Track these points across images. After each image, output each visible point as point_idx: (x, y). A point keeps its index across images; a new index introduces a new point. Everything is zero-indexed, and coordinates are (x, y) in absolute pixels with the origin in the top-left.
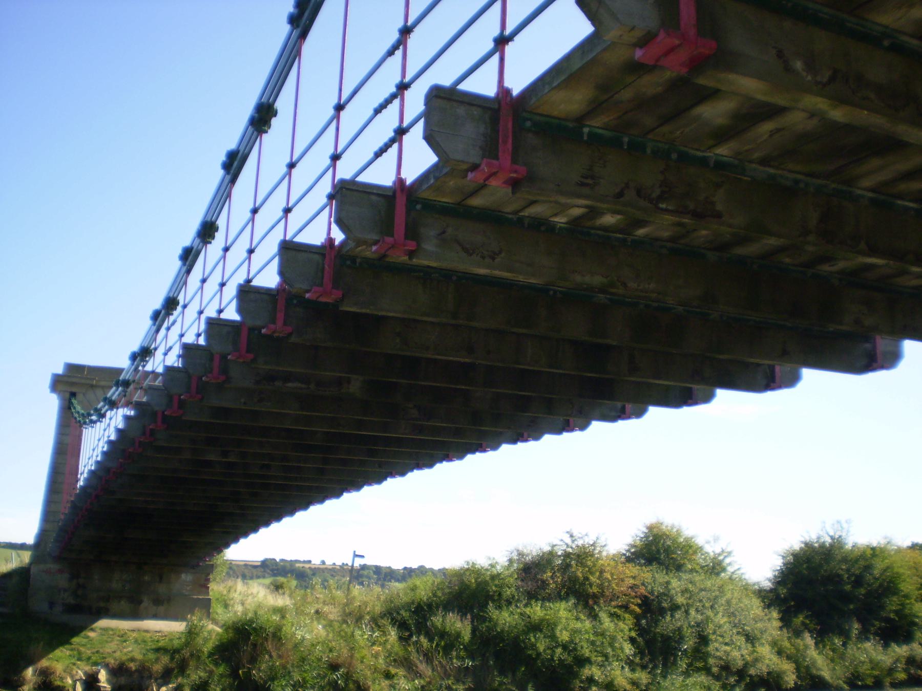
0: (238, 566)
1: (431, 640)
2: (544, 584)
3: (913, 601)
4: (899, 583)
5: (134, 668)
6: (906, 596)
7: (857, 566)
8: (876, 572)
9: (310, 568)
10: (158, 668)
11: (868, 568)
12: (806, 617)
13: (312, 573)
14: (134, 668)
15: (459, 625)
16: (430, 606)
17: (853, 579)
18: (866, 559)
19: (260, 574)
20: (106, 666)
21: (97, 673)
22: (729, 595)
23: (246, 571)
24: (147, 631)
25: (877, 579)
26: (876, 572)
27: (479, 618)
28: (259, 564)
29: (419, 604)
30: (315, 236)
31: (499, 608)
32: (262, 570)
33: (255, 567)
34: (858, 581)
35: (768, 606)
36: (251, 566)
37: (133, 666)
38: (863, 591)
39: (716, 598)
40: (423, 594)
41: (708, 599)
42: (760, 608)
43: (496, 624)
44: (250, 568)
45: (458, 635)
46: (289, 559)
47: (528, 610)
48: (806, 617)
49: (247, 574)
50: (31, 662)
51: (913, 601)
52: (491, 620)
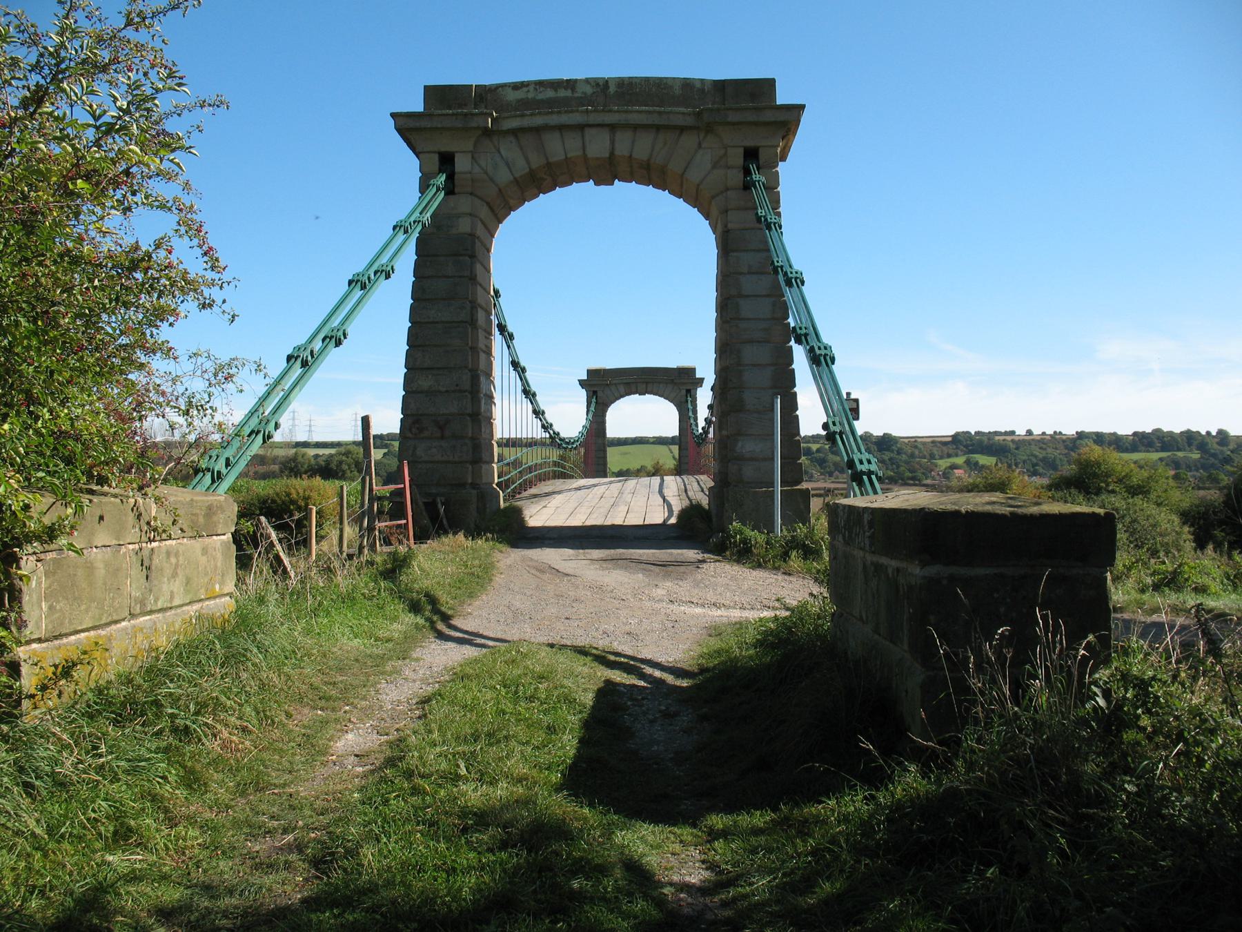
0: (924, 444)
28: (950, 439)
33: (945, 444)
44: (939, 445)
46: (987, 431)
49: (936, 452)
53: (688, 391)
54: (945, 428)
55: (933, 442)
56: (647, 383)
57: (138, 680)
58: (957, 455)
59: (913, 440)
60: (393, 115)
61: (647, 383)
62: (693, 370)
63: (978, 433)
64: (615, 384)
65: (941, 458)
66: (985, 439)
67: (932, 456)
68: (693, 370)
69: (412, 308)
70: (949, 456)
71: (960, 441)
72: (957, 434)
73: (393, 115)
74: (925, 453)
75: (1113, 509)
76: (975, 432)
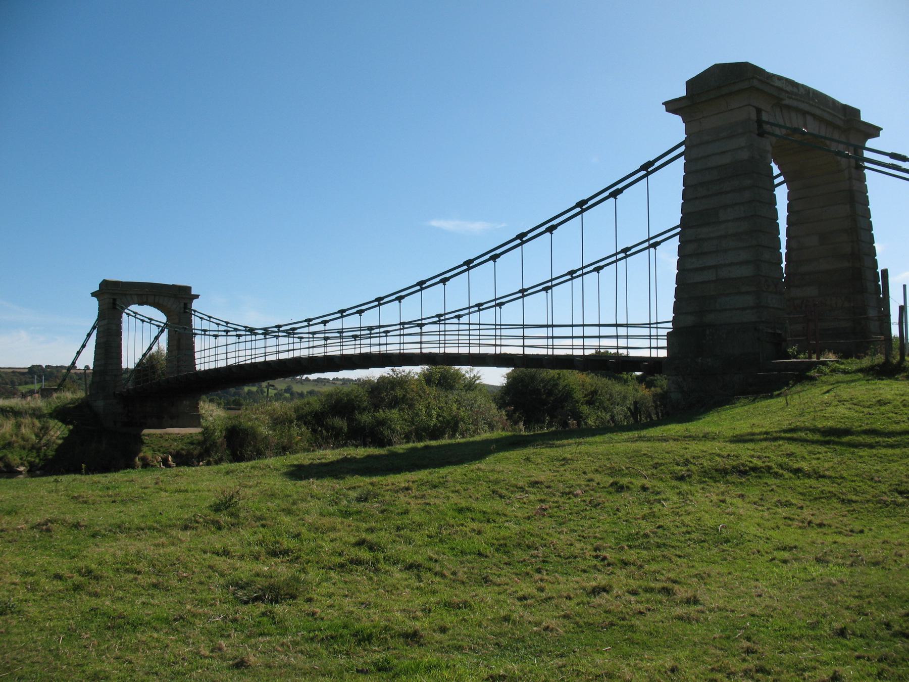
0: (6, 373)
1: (328, 432)
2: (383, 399)
3: (580, 404)
4: (573, 394)
5: (185, 453)
6: (577, 402)
7: (549, 385)
8: (560, 388)
9: (75, 373)
10: (196, 452)
11: (556, 385)
12: (520, 413)
13: (78, 378)
14: (185, 453)
15: (340, 423)
16: (322, 413)
17: (547, 391)
18: (554, 380)
19: (28, 380)
20: (170, 453)
21: (168, 457)
22: (479, 403)
23: (15, 379)
24: (169, 434)
25: (560, 391)
26: (560, 388)
27: (351, 420)
28: (27, 370)
29: (316, 413)
30: (644, 386)
31: (360, 413)
32: (31, 376)
33: (23, 374)
34: (550, 393)
35: (500, 408)
36: (19, 373)
37: (184, 452)
38: (552, 398)
39: (473, 404)
40: (317, 407)
41: (469, 404)
42: (496, 409)
43: (360, 422)
44: (18, 374)
45: (341, 428)
46: (54, 365)
47: (377, 414)
48: (520, 413)
49: (16, 380)
50: (136, 454)
51: (580, 404)
52: (356, 420)
53: (185, 304)
54: (24, 362)
55: (13, 372)
56: (155, 295)
57: (9, 611)
58: (33, 383)
59: (11, 370)
60: (663, 104)
61: (155, 295)
62: (189, 288)
63: (48, 367)
64: (131, 294)
65: (20, 384)
66: (55, 371)
67: (13, 383)
68: (189, 288)
69: (788, 217)
70: (26, 383)
71: (35, 373)
72: (33, 367)
73: (663, 104)
74: (7, 380)
75: (781, 393)
76: (46, 366)
